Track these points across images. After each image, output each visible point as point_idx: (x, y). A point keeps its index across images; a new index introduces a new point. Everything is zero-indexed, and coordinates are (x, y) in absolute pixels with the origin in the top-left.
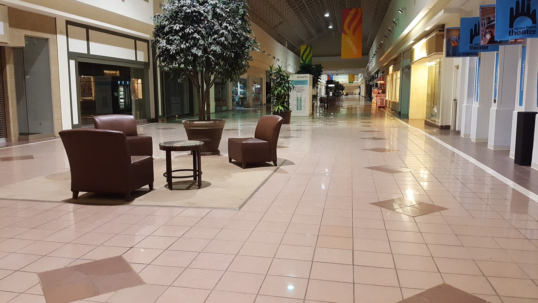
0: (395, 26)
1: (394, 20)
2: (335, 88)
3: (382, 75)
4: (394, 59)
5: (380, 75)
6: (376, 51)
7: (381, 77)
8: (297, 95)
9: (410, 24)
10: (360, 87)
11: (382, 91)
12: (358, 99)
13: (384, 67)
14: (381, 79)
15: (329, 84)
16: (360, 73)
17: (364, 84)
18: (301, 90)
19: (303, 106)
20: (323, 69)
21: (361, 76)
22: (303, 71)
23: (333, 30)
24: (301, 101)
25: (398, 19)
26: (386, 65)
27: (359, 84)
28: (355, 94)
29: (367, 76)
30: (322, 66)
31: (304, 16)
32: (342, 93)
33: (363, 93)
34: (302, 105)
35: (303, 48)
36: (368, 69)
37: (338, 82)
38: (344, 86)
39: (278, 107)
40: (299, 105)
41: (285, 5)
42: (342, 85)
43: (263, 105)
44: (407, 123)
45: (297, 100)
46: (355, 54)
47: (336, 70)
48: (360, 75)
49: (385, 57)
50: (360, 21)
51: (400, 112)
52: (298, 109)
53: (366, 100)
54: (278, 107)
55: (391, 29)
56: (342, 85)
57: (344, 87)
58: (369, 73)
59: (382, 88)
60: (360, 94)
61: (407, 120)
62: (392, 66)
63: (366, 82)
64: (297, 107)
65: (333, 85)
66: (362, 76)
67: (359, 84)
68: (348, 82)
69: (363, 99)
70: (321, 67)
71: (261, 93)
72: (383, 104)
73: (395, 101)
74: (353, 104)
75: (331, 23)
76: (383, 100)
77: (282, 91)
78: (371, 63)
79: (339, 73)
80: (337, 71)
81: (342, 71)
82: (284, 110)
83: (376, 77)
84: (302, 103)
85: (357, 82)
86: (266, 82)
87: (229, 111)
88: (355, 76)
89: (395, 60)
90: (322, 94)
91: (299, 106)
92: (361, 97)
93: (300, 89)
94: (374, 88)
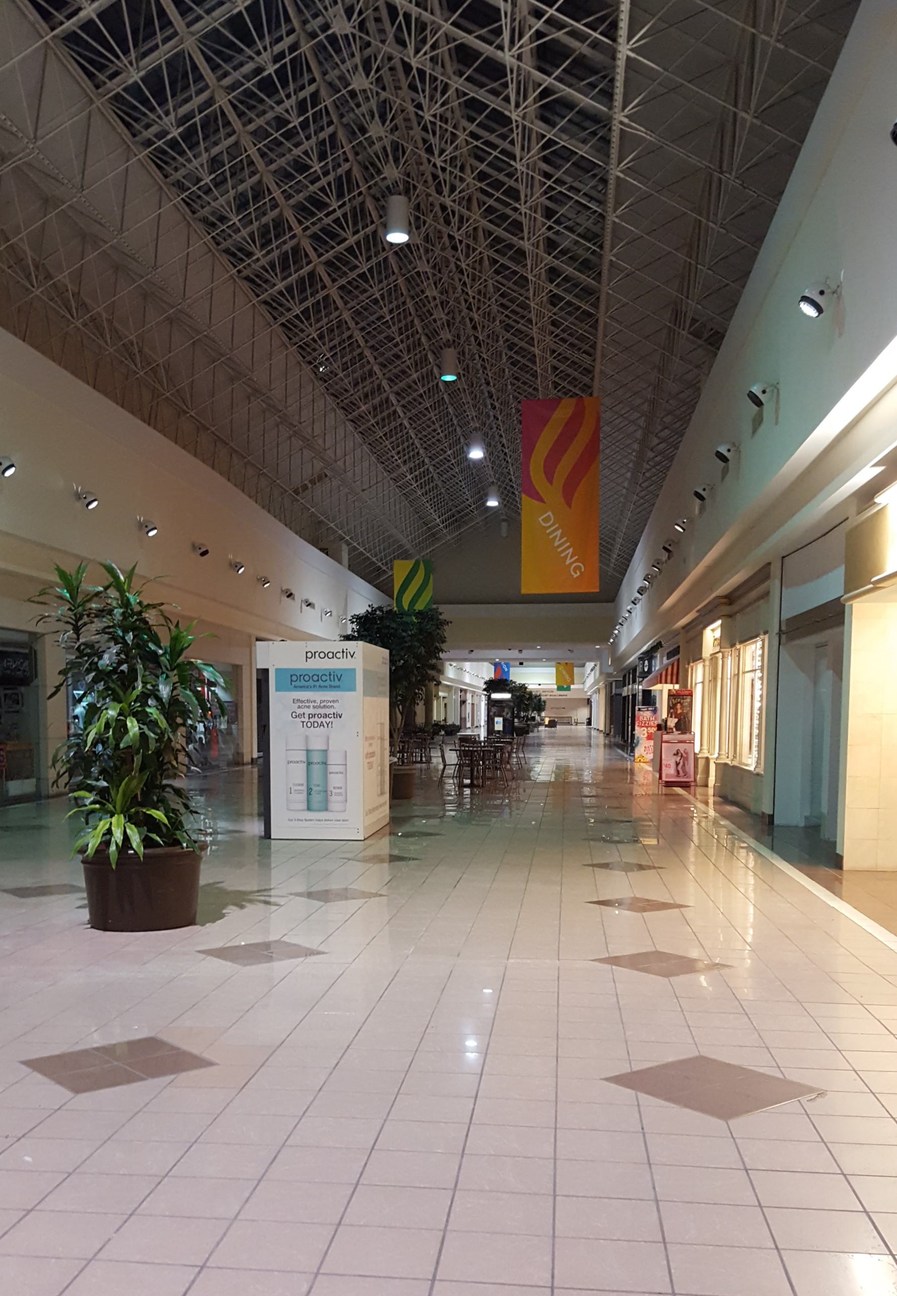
0: (747, 427)
1: (756, 390)
2: (512, 704)
3: (665, 661)
4: (726, 597)
5: (659, 663)
6: (647, 575)
7: (667, 670)
8: (307, 738)
9: (887, 344)
10: (589, 702)
11: (676, 720)
12: (585, 740)
13: (676, 633)
14: (669, 678)
15: (494, 692)
16: (591, 660)
17: (603, 694)
18: (326, 716)
19: (334, 791)
20: (447, 631)
21: (592, 670)
22: (365, 633)
23: (504, 520)
24: (326, 769)
25: (776, 387)
26: (684, 628)
27: (586, 692)
28: (577, 723)
29: (611, 670)
30: (441, 617)
31: (399, 453)
32: (538, 718)
33: (600, 720)
34: (331, 788)
35: (400, 571)
36: (615, 645)
37: (523, 687)
38: (543, 698)
39: (103, 826)
40: (315, 789)
41: (311, 397)
42: (536, 696)
43: (248, 764)
44: (833, 886)
45: (309, 764)
46: (575, 576)
47: (515, 649)
48: (590, 665)
49: (685, 595)
50: (591, 452)
51: (771, 817)
52: (315, 805)
53: (610, 746)
54: (103, 826)
55: (729, 450)
56: (538, 697)
57: (544, 702)
58: (618, 660)
59: (679, 711)
60: (589, 723)
61: (832, 872)
62: (719, 622)
63: (609, 686)
64: (309, 794)
65: (507, 696)
66: (598, 668)
67: (586, 692)
68: (555, 687)
69: (601, 739)
70: (438, 619)
71: (237, 720)
72: (686, 774)
73: (735, 763)
74: (571, 757)
75: (493, 489)
76: (686, 759)
77: (133, 726)
78: (625, 626)
79: (527, 660)
80: (520, 651)
81: (535, 651)
82: (147, 842)
83: (646, 669)
84: (331, 777)
85: (581, 686)
86: (452, 687)
87: (48, 797)
88: (575, 669)
89: (730, 598)
90: (479, 721)
91: (319, 793)
92: (594, 733)
93: (322, 711)
94: (639, 710)
